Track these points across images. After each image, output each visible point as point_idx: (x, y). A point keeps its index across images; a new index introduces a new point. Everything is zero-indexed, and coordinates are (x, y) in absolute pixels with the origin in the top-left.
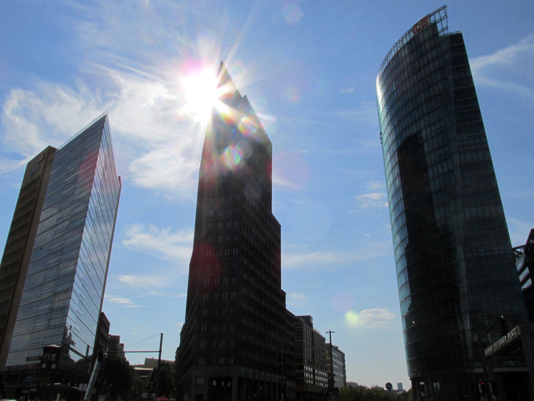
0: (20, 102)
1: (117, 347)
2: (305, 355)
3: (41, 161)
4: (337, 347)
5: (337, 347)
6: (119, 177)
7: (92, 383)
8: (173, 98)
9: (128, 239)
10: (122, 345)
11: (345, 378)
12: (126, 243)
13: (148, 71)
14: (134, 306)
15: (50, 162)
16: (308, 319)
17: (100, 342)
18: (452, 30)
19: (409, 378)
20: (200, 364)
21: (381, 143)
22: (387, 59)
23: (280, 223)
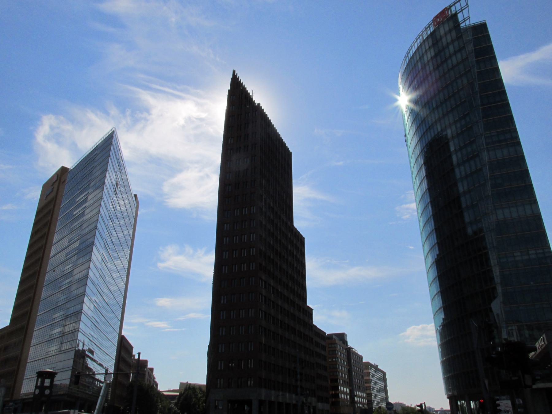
0: (52, 128)
1: (145, 372)
2: (339, 375)
3: (55, 182)
4: (377, 366)
5: (377, 366)
6: (136, 196)
7: (99, 410)
8: (204, 115)
9: (163, 261)
10: (152, 370)
11: (387, 398)
12: (161, 265)
13: (181, 91)
14: (172, 330)
15: (63, 182)
16: (342, 337)
17: (122, 366)
18: (475, 20)
19: (446, 396)
20: (219, 386)
21: (407, 145)
22: (408, 56)
23: (304, 236)
